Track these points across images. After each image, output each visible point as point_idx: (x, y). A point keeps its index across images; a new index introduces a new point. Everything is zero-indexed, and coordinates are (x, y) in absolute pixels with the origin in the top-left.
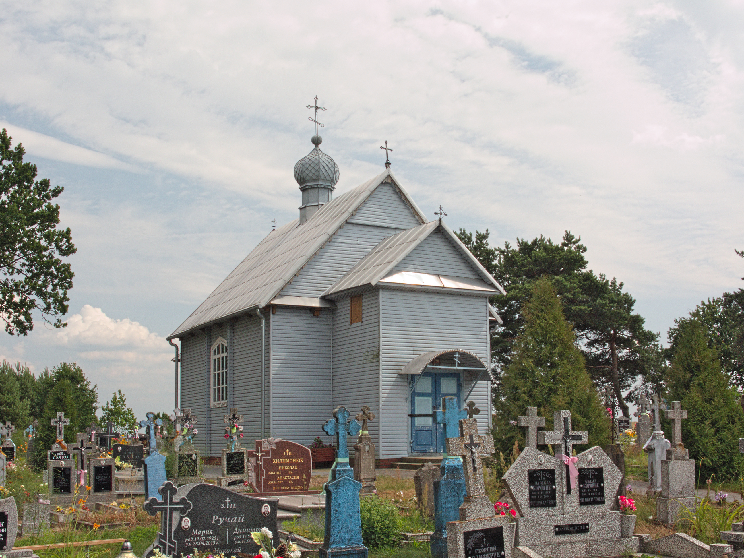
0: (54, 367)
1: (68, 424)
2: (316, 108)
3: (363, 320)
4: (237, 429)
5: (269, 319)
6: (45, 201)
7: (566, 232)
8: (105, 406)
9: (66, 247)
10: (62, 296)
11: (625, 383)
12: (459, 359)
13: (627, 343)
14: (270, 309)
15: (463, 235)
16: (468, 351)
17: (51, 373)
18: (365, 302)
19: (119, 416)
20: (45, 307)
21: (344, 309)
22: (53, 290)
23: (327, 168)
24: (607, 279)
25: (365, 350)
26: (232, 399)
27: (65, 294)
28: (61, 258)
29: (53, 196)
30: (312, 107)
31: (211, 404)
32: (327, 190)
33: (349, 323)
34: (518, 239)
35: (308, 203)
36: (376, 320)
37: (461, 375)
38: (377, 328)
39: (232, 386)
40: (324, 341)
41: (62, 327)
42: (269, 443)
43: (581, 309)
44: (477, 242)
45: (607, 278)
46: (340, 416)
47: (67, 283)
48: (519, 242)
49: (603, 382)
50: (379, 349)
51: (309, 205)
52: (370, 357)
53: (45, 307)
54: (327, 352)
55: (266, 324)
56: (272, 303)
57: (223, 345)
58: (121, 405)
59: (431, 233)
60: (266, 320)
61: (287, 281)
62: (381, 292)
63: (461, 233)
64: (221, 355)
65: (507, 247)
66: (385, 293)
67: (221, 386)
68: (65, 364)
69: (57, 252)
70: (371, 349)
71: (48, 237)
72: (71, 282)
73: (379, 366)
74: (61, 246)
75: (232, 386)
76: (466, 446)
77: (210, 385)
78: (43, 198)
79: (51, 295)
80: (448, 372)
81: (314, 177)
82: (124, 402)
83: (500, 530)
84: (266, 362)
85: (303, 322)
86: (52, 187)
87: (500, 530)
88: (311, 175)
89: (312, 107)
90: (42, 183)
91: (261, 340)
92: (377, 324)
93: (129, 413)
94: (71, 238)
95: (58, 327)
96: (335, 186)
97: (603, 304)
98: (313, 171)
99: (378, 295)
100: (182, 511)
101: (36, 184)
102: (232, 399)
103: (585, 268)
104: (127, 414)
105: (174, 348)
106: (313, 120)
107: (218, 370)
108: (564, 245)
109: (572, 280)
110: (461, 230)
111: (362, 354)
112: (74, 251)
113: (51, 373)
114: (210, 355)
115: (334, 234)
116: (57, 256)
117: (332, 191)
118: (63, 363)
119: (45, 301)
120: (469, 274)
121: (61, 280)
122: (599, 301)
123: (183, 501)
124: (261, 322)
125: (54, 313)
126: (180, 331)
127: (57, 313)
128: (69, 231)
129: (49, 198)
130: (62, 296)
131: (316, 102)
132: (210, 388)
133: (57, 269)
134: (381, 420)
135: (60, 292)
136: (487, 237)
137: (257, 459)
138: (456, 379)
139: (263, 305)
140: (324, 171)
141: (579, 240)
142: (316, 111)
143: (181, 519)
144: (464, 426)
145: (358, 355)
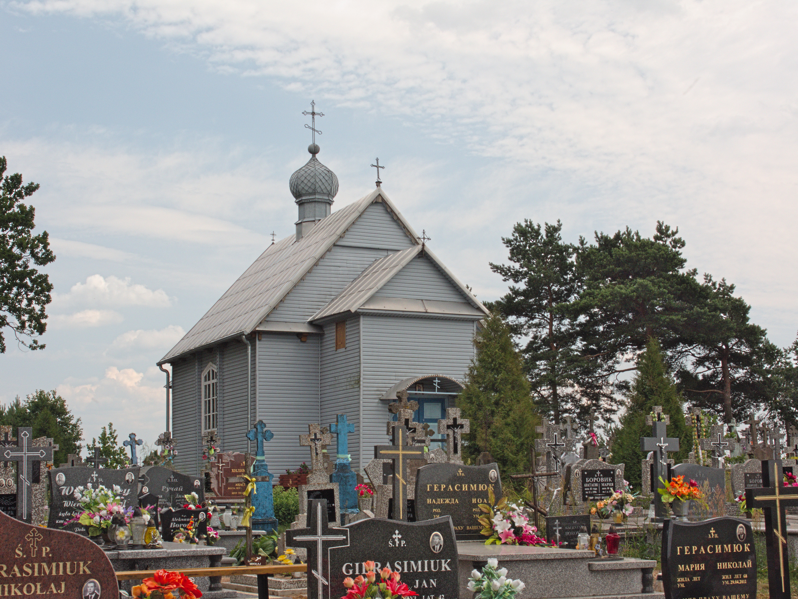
0: (28, 395)
1: (57, 449)
2: (313, 114)
3: (347, 346)
4: (215, 450)
5: (255, 345)
6: (17, 200)
7: (658, 222)
8: (91, 444)
9: (43, 254)
10: (39, 313)
11: (746, 412)
12: (439, 384)
13: (741, 361)
14: (254, 336)
15: (530, 227)
16: (448, 376)
17: (24, 403)
18: (349, 328)
19: (109, 456)
20: (19, 325)
21: (330, 334)
22: (29, 305)
23: (323, 180)
24: (714, 281)
25: (348, 376)
26: (222, 427)
27: (42, 310)
28: (36, 267)
29: (27, 194)
30: (308, 113)
31: (203, 433)
32: (324, 204)
33: (334, 349)
34: (596, 233)
35: (304, 218)
36: (357, 346)
37: (446, 400)
38: (357, 354)
39: (222, 413)
40: (310, 367)
41: (38, 349)
42: (229, 455)
43: (672, 320)
44: (547, 236)
45: (714, 279)
46: (259, 427)
47: (44, 296)
48: (597, 236)
49: (719, 411)
50: (360, 375)
51: (305, 220)
52: (353, 383)
53: (19, 325)
54: (314, 378)
55: (251, 350)
56: (257, 329)
57: (213, 371)
58: (112, 442)
59: (415, 258)
60: (252, 346)
61: (272, 307)
62: (362, 319)
63: (527, 226)
64: (212, 382)
65: (582, 243)
66: (366, 319)
67: (211, 414)
68: (41, 392)
69: (32, 261)
70: (353, 375)
71: (22, 246)
72: (49, 295)
73: (359, 391)
74: (37, 253)
75: (222, 413)
76: (312, 440)
77: (201, 412)
78: (14, 196)
79: (26, 311)
80: (431, 397)
81: (310, 191)
82: (115, 439)
83: (332, 491)
84: (252, 389)
85: (287, 347)
86: (25, 183)
87: (332, 491)
88: (306, 188)
89: (308, 113)
90: (12, 178)
91: (247, 366)
92: (358, 350)
93: (121, 452)
94: (48, 244)
95: (34, 348)
96: (334, 199)
97: (701, 312)
98: (309, 184)
99: (359, 321)
100: (143, 483)
101: (6, 180)
102: (222, 427)
103: (682, 268)
104: (118, 454)
105: (165, 374)
106: (309, 127)
107: (209, 397)
108: (656, 238)
109: (661, 284)
110: (526, 221)
111: (345, 380)
112: (52, 259)
113: (24, 403)
114: (201, 382)
115: (322, 257)
116: (32, 265)
117: (330, 204)
118: (39, 391)
119: (19, 318)
120: (455, 298)
121: (36, 293)
122: (696, 309)
123: (143, 476)
124: (247, 348)
125: (29, 332)
126: (171, 356)
127: (32, 333)
128: (45, 235)
129: (22, 197)
130: (39, 313)
131: (313, 107)
132: (201, 416)
133: (32, 281)
134: (361, 445)
135: (37, 308)
136: (560, 230)
137: (219, 469)
138: (440, 404)
139: (248, 331)
140: (320, 183)
141: (677, 232)
142: (313, 118)
143: (142, 487)
144: (311, 428)
145: (342, 381)
